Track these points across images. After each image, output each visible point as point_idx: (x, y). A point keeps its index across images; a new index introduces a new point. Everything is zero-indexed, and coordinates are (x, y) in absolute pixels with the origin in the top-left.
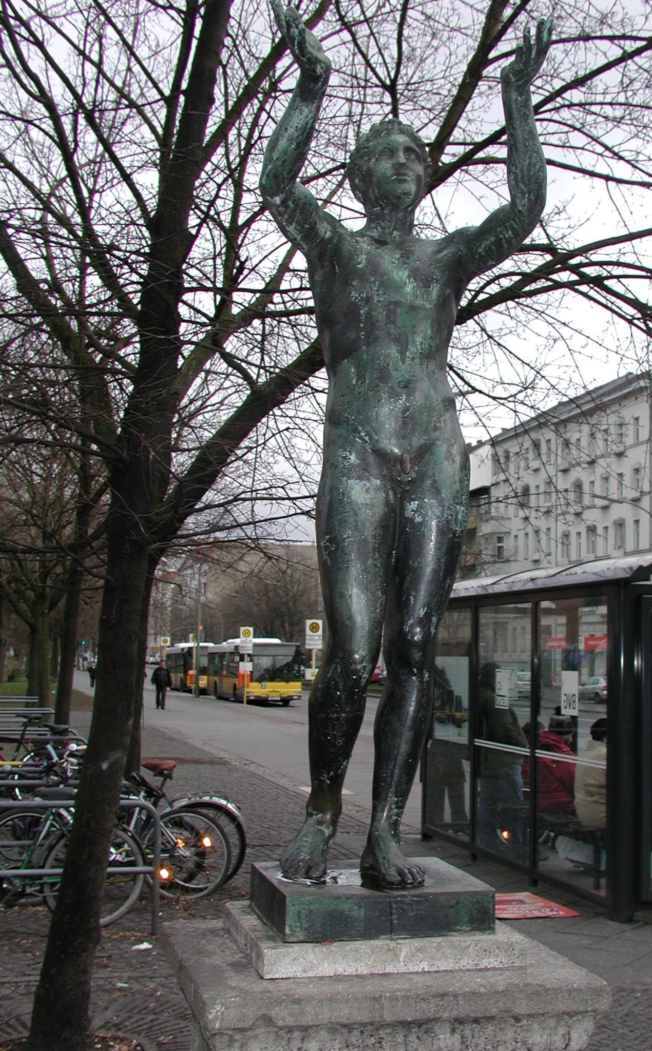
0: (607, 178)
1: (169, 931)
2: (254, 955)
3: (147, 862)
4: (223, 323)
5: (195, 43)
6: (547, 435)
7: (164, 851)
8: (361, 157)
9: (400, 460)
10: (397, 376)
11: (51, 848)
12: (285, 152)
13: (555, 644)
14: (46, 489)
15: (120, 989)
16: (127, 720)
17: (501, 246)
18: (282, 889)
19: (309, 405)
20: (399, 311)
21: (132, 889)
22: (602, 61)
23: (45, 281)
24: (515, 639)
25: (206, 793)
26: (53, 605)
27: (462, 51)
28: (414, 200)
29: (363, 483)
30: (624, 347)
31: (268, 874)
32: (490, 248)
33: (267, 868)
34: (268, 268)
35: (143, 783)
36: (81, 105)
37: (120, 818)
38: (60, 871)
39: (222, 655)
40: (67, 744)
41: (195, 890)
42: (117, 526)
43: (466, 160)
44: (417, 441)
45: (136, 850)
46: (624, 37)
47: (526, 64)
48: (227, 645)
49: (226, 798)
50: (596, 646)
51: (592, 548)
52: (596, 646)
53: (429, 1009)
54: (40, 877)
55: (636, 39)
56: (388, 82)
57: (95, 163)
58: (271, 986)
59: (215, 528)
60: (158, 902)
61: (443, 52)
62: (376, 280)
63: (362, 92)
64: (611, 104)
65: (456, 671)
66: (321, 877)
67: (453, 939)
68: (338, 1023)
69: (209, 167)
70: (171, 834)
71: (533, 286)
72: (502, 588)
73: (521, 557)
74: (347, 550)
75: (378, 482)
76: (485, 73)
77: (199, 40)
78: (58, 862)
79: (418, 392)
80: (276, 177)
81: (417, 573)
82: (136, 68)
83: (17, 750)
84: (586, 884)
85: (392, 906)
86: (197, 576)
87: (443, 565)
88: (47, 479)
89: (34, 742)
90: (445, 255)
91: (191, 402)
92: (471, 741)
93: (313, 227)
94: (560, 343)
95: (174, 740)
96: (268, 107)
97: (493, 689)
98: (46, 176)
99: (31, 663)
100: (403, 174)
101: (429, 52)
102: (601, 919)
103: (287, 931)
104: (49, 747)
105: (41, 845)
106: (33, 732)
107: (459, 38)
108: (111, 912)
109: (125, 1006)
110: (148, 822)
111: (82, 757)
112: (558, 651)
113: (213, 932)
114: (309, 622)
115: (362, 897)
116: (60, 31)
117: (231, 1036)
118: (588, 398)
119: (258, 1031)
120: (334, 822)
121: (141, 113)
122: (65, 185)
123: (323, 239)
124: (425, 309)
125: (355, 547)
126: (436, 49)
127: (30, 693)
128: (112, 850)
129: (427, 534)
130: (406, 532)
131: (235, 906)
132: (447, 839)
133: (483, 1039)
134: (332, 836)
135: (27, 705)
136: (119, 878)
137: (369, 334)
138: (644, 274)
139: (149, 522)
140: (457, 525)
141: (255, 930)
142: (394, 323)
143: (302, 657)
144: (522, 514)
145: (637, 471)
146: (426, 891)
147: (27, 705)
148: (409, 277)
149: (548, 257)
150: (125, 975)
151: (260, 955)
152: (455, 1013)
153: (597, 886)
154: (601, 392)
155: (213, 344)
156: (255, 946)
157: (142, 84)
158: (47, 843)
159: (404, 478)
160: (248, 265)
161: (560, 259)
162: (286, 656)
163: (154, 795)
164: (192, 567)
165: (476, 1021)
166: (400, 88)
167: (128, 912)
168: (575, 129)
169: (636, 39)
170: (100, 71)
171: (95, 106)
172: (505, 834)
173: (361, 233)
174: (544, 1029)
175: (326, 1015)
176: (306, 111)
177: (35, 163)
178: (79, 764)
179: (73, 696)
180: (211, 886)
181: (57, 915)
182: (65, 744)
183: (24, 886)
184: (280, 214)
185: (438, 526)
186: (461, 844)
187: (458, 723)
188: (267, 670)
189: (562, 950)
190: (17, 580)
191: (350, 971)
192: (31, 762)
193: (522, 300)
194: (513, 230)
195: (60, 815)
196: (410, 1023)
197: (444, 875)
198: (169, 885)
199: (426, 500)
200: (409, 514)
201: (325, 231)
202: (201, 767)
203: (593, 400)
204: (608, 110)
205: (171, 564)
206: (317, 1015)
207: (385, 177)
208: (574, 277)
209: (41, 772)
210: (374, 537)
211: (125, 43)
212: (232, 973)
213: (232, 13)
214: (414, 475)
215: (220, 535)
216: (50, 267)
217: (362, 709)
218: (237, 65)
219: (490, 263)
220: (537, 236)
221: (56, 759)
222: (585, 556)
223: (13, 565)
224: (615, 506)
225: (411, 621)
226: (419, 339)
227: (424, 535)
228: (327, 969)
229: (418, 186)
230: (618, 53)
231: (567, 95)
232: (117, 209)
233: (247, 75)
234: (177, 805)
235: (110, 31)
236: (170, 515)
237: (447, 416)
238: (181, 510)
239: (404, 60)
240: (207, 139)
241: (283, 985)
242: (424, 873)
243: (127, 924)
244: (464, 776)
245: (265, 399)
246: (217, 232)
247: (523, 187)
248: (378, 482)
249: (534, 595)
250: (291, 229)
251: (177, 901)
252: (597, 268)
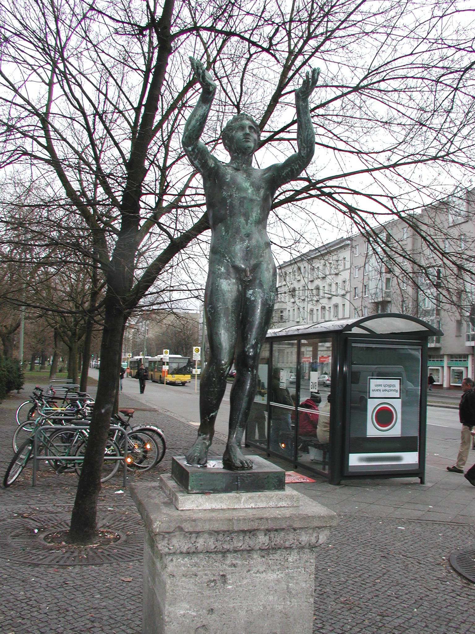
0: (334, 149)
1: (134, 487)
2: (174, 499)
3: (122, 455)
4: (158, 211)
5: (149, 86)
6: (304, 265)
7: (129, 450)
8: (229, 130)
9: (244, 271)
10: (243, 232)
11: (79, 447)
12: (194, 127)
13: (306, 360)
14: (77, 285)
16: (113, 390)
17: (294, 172)
18: (187, 469)
19: (202, 246)
20: (245, 201)
21: (115, 467)
22: (334, 96)
23: (79, 191)
24: (288, 357)
25: (148, 424)
26: (79, 338)
27: (269, 91)
28: (253, 151)
29: (227, 281)
30: (341, 225)
31: (180, 462)
33: (179, 459)
34: (180, 186)
35: (119, 419)
36: (97, 112)
37: (109, 435)
38: (83, 457)
39: (155, 362)
40: (86, 401)
41: (143, 468)
42: (109, 301)
43: (271, 139)
44: (253, 262)
45: (117, 449)
46: (343, 86)
47: (307, 88)
48: (157, 358)
49: (157, 427)
50: (325, 361)
51: (323, 316)
52: (325, 361)
53: (255, 525)
54: (74, 460)
55: (348, 87)
56: (236, 103)
57: (102, 138)
58: (182, 513)
59: (153, 304)
60: (126, 473)
61: (261, 91)
63: (224, 108)
64: (337, 115)
65: (263, 372)
66: (205, 464)
67: (266, 493)
68: (213, 531)
69: (155, 138)
70: (132, 442)
71: (300, 196)
72: (283, 333)
73: (291, 318)
74: (220, 312)
75: (234, 281)
76: (280, 100)
77: (151, 84)
78: (82, 454)
79: (253, 239)
80: (190, 138)
81: (251, 324)
82: (122, 96)
83: (63, 403)
84: (319, 468)
85: (238, 478)
86: (144, 326)
87: (264, 321)
88: (78, 281)
89: (71, 399)
91: (143, 246)
92: (268, 402)
93: (206, 162)
94: (312, 222)
95: (133, 400)
96: (182, 112)
97: (279, 379)
98: (80, 144)
99: (69, 364)
100: (248, 139)
101: (254, 90)
102: (326, 483)
103: (189, 488)
104: (78, 402)
105: (74, 446)
106: (70, 395)
107: (268, 84)
108: (105, 476)
110: (122, 437)
111: (92, 407)
112: (307, 363)
113: (154, 487)
114: (194, 348)
115: (224, 473)
117: (164, 535)
118: (324, 248)
119: (176, 533)
120: (211, 439)
121: (124, 116)
122: (89, 148)
123: (210, 167)
124: (257, 200)
125: (223, 311)
126: (257, 90)
127: (69, 377)
128: (106, 449)
129: (257, 306)
130: (243, 306)
131: (165, 476)
132: (257, 447)
133: (279, 538)
134: (210, 445)
135: (68, 383)
136: (109, 461)
137: (231, 212)
138: (350, 192)
139: (124, 299)
141: (174, 488)
142: (243, 206)
143: (191, 364)
144: (292, 300)
145: (344, 282)
146: (253, 471)
147: (68, 383)
148: (250, 186)
149: (307, 184)
151: (177, 499)
152: (267, 527)
153: (324, 469)
154: (329, 245)
155: (154, 220)
156: (174, 494)
157: (125, 104)
158: (77, 445)
159: (247, 279)
160: (171, 185)
161: (312, 185)
162: (184, 363)
163: (125, 425)
164: (142, 322)
165: (276, 530)
166: (241, 106)
167: (113, 477)
168: (320, 126)
169: (348, 87)
170: (106, 98)
171: (104, 113)
172: (283, 445)
173: (228, 165)
174: (307, 534)
175: (207, 527)
176: (204, 108)
177: (76, 138)
178: (91, 410)
179: (88, 379)
180: (150, 466)
181: (82, 478)
182: (85, 401)
183: (67, 464)
184: (191, 155)
185: (262, 302)
186: (263, 449)
187: (262, 395)
188: (175, 369)
189: (313, 497)
190: (64, 326)
191: (218, 507)
192: (69, 408)
193: (294, 203)
194: (299, 165)
195: (83, 433)
196: (246, 531)
197: (260, 463)
198: (131, 465)
200: (248, 296)
201: (212, 164)
202: (145, 412)
203: (326, 249)
204: (335, 118)
205: (132, 321)
206: (203, 526)
207: (239, 139)
208: (319, 193)
209: (74, 413)
210: (232, 306)
211: (117, 84)
212: (164, 507)
213: (167, 71)
214: (251, 278)
215: (155, 307)
216: (81, 184)
217: (225, 387)
218: (169, 93)
220: (303, 175)
221: (81, 407)
222: (320, 320)
223: (62, 320)
224: (334, 298)
225: (248, 346)
226: (254, 215)
227: (255, 306)
228: (208, 506)
229: (255, 144)
230: (340, 93)
231: (317, 111)
232: (112, 160)
233: (173, 98)
234: (135, 429)
235: (111, 80)
236: (134, 297)
237: (267, 251)
238: (139, 295)
239: (243, 94)
240: (154, 126)
241: (188, 513)
242: (252, 463)
243: (112, 482)
244: (265, 419)
245: (177, 246)
246: (157, 169)
249: (299, 337)
250: (196, 162)
251: (135, 472)
252: (329, 189)
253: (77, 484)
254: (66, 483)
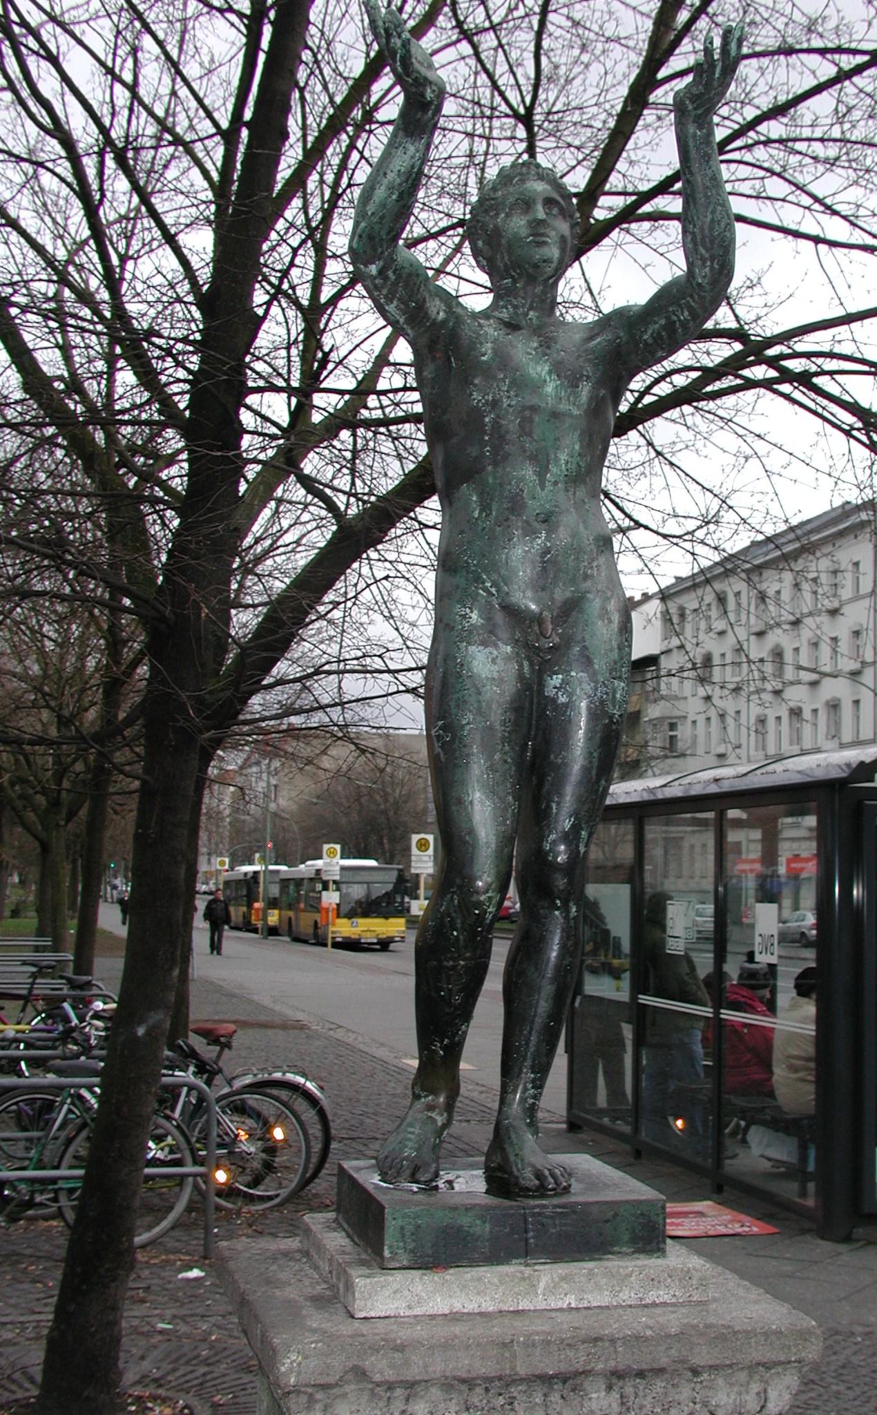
0: (817, 240)
1: (227, 1253)
2: (341, 1286)
3: (197, 1161)
4: (300, 436)
5: (262, 58)
6: (735, 585)
7: (220, 1146)
8: (486, 211)
9: (538, 620)
10: (533, 506)
11: (69, 1141)
12: (383, 205)
13: (746, 867)
14: (62, 658)
16: (171, 969)
17: (674, 331)
18: (380, 1197)
19: (416, 546)
20: (537, 419)
21: (178, 1197)
22: (810, 83)
23: (60, 378)
24: (692, 860)
25: (277, 1068)
26: (71, 815)
27: (621, 68)
28: (556, 270)
29: (488, 650)
30: (840, 467)
31: (360, 1177)
32: (659, 333)
33: (359, 1169)
34: (361, 361)
35: (193, 1054)
36: (109, 141)
37: (161, 1102)
38: (81, 1172)
39: (299, 882)
40: (91, 1002)
41: (262, 1199)
42: (157, 708)
43: (627, 216)
44: (561, 594)
45: (184, 1145)
46: (839, 50)
47: (708, 86)
48: (306, 869)
49: (304, 1075)
50: (802, 869)
51: (797, 737)
52: (802, 869)
53: (578, 1359)
54: (54, 1181)
55: (855, 52)
56: (522, 111)
57: (128, 219)
58: (364, 1328)
59: (290, 711)
60: (213, 1215)
61: (597, 69)
62: (505, 377)
63: (487, 124)
64: (822, 140)
65: (614, 903)
66: (432, 1180)
67: (609, 1264)
68: (454, 1378)
69: (281, 225)
70: (230, 1123)
71: (717, 386)
72: (676, 791)
73: (700, 750)
74: (467, 740)
75: (509, 649)
76: (652, 98)
77: (268, 53)
78: (78, 1161)
79: (562, 528)
80: (371, 238)
81: (560, 772)
82: (183, 92)
83: (23, 1010)
84: (788, 1190)
85: (527, 1220)
86: (265, 776)
87: (595, 761)
88: (63, 644)
89: (46, 998)
90: (599, 343)
91: (258, 541)
92: (634, 997)
93: (421, 306)
94: (754, 462)
95: (234, 996)
96: (360, 144)
97: (663, 928)
98: (61, 237)
99: (41, 893)
100: (543, 235)
101: (577, 70)
102: (808, 1237)
103: (387, 1253)
104: (66, 1005)
105: (56, 1138)
106: (45, 986)
107: (617, 51)
108: (149, 1228)
110: (200, 1107)
111: (110, 1019)
112: (751, 876)
113: (286, 1254)
114: (415, 838)
115: (487, 1208)
117: (311, 1395)
118: (791, 536)
119: (347, 1388)
120: (449, 1107)
121: (190, 152)
122: (87, 249)
123: (434, 322)
124: (571, 416)
125: (478, 737)
126: (587, 66)
127: (40, 933)
128: (151, 1144)
129: (575, 719)
130: (547, 716)
131: (316, 1220)
132: (602, 1129)
133: (649, 1398)
134: (447, 1125)
135: (37, 949)
136: (160, 1183)
137: (496, 450)
138: (866, 368)
139: (200, 703)
140: (614, 706)
141: (344, 1253)
142: (530, 435)
143: (406, 885)
144: (702, 692)
145: (857, 633)
146: (573, 1199)
147: (37, 949)
148: (550, 372)
149: (738, 347)
151: (349, 1286)
152: (613, 1363)
153: (803, 1193)
154: (808, 527)
155: (287, 463)
156: (343, 1273)
157: (191, 114)
158: (63, 1134)
159: (543, 644)
160: (334, 357)
161: (754, 349)
162: (384, 883)
163: (206, 1070)
164: (258, 763)
165: (641, 1374)
166: (538, 118)
167: (172, 1228)
168: (773, 173)
169: (855, 52)
170: (135, 96)
171: (127, 142)
172: (680, 1123)
173: (485, 314)
174: (731, 1385)
175: (439, 1366)
176: (412, 149)
177: (47, 219)
178: (106, 1029)
179: (98, 937)
180: (284, 1193)
181: (77, 1232)
182: (88, 1002)
183: (33, 1193)
184: (376, 287)
185: (589, 709)
186: (620, 1136)
187: (616, 974)
188: (359, 902)
189: (756, 1279)
190: (23, 781)
191: (471, 1307)
192: (42, 1026)
193: (702, 404)
194: (690, 309)
195: (81, 1098)
196: (552, 1377)
197: (597, 1177)
198: (228, 1192)
199: (573, 674)
200: (550, 692)
201: (437, 311)
202: (270, 1032)
203: (798, 539)
204: (818, 148)
205: (230, 760)
206: (426, 1366)
207: (517, 239)
208: (772, 373)
209: (56, 1040)
210: (504, 723)
211: (168, 57)
212: (312, 1311)
213: (312, 17)
214: (557, 640)
215: (295, 720)
216: (68, 359)
217: (487, 954)
218: (319, 88)
219: (659, 354)
220: (723, 318)
221: (75, 1021)
222: (786, 748)
223: (17, 760)
224: (827, 682)
225: (553, 837)
226: (563, 457)
227: (570, 721)
228: (440, 1305)
229: (563, 250)
230: (832, 71)
231: (762, 128)
232: (157, 281)
233: (332, 101)
234: (238, 1084)
235: (147, 42)
236: (228, 693)
237: (602, 560)
238: (244, 687)
239: (544, 81)
240: (279, 186)
241: (381, 1327)
242: (570, 1175)
243: (171, 1244)
244: (624, 1045)
245: (357, 537)
246: (292, 313)
247: (703, 251)
248: (509, 649)
249: (718, 801)
250: (391, 308)
251: (239, 1213)
252: (803, 360)
253: (62, 1253)
254: (28, 1251)
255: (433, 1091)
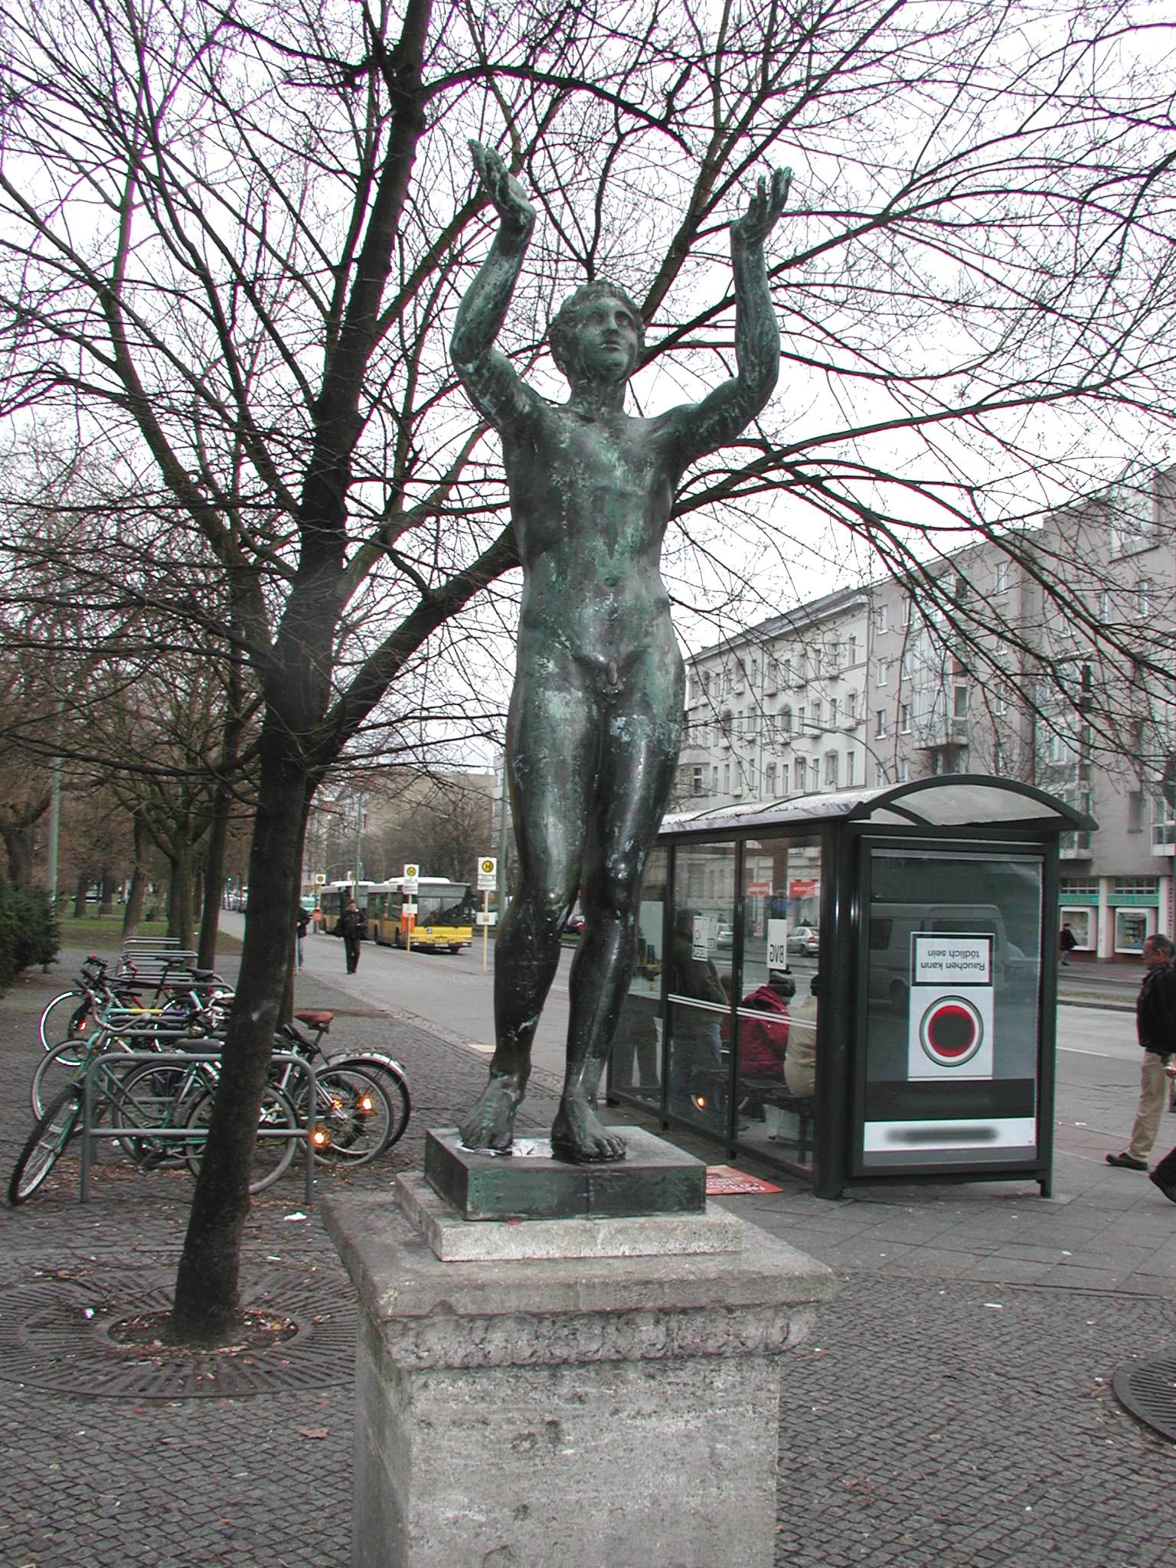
0: (828, 368)
1: (332, 1204)
2: (430, 1234)
3: (301, 1125)
4: (392, 521)
5: (368, 212)
6: (752, 655)
7: (319, 1113)
8: (566, 323)
9: (605, 669)
10: (602, 573)
11: (195, 1106)
12: (480, 313)
13: (757, 889)
14: (191, 704)
15: (271, 1263)
16: (281, 965)
17: (727, 426)
18: (464, 1160)
19: (499, 608)
20: (607, 497)
21: (284, 1154)
22: (826, 237)
23: (195, 472)
24: (712, 883)
25: (367, 1050)
26: (197, 836)
27: (666, 224)
28: (626, 372)
29: (563, 694)
30: (843, 555)
31: (446, 1143)
33: (444, 1136)
34: (445, 460)
35: (296, 1037)
36: (240, 276)
37: (271, 1075)
38: (205, 1131)
39: (383, 896)
40: (212, 992)
41: (353, 1157)
42: (271, 745)
43: (670, 343)
44: (626, 648)
45: (289, 1112)
46: (848, 214)
47: (760, 218)
48: (390, 885)
49: (388, 1055)
50: (804, 892)
51: (801, 782)
52: (804, 892)
53: (631, 1299)
54: (183, 1137)
55: (861, 216)
56: (584, 256)
57: (254, 342)
58: (451, 1270)
59: (378, 752)
60: (313, 1169)
61: (646, 224)
63: (554, 267)
64: (834, 285)
65: (651, 919)
66: (507, 1147)
67: (658, 1219)
68: (526, 1312)
69: (383, 342)
70: (328, 1094)
71: (743, 486)
72: (702, 825)
73: (721, 788)
74: (543, 773)
75: (580, 694)
76: (692, 248)
77: (374, 209)
78: (202, 1123)
79: (627, 592)
80: (469, 341)
81: (622, 800)
82: (303, 238)
83: (157, 997)
84: (790, 1157)
85: (590, 1183)
86: (356, 807)
87: (653, 793)
88: (192, 694)
89: (175, 987)
91: (354, 609)
92: (664, 995)
93: (510, 400)
94: (772, 550)
95: (330, 989)
96: (451, 277)
97: (690, 938)
98: (198, 357)
99: (171, 901)
100: (615, 343)
101: (630, 223)
102: (806, 1196)
103: (469, 1208)
104: (192, 993)
105: (184, 1103)
106: (174, 977)
107: (663, 209)
108: (260, 1178)
109: (277, 1282)
110: (301, 1081)
111: (228, 1006)
112: (761, 898)
113: (381, 1206)
114: (481, 860)
115: (554, 1171)
116: (219, 198)
117: (405, 1324)
118: (802, 613)
119: (436, 1319)
120: (522, 1086)
121: (306, 286)
122: (219, 366)
123: (521, 413)
124: (637, 496)
125: (552, 770)
126: (637, 222)
127: (171, 933)
128: (263, 1110)
129: (635, 756)
130: (603, 756)
131: (408, 1178)
132: (636, 1105)
133: (691, 1331)
134: (519, 1101)
135: (168, 947)
136: (270, 1141)
137: (571, 524)
138: (866, 474)
139: (307, 740)
141: (431, 1206)
142: (601, 510)
143: (473, 899)
144: (724, 742)
145: (852, 697)
146: (627, 1165)
147: (168, 947)
148: (619, 459)
149: (759, 454)
150: (277, 1248)
151: (437, 1234)
152: (660, 1303)
153: (802, 1160)
154: (816, 606)
155: (382, 544)
156: (431, 1223)
157: (309, 256)
158: (190, 1100)
159: (610, 691)
160: (423, 456)
161: (773, 457)
162: (454, 898)
163: (309, 1050)
164: (350, 797)
165: (684, 1311)
166: (597, 262)
167: (279, 1179)
168: (793, 311)
169: (861, 216)
170: (263, 242)
171: (256, 279)
172: (701, 1101)
173: (564, 408)
174: (760, 1320)
175: (513, 1303)
176: (506, 266)
177: (187, 342)
178: (225, 1014)
179: (218, 938)
180: (371, 1152)
181: (203, 1183)
182: (209, 992)
183: (165, 1147)
184: (473, 383)
185: (648, 746)
186: (651, 1111)
187: (649, 976)
188: (433, 913)
189: (775, 1230)
190: (158, 807)
191: (541, 1253)
192: (172, 1010)
193: (729, 501)
194: (741, 407)
195: (204, 1070)
196: (609, 1313)
197: (645, 1146)
198: (325, 1151)
200: (614, 731)
201: (524, 405)
202: (359, 1020)
203: (808, 615)
204: (829, 293)
205: (328, 794)
206: (503, 1302)
207: (592, 345)
208: (789, 477)
209: (184, 1022)
210: (575, 758)
211: (291, 208)
212: (405, 1254)
213: (413, 174)
214: (621, 687)
215: (383, 760)
216: (201, 456)
217: (556, 956)
218: (417, 231)
220: (751, 432)
221: (200, 1007)
222: (792, 791)
223: (153, 790)
224: (827, 736)
225: (615, 856)
226: (629, 531)
227: (631, 757)
228: (514, 1251)
229: (631, 356)
230: (843, 231)
231: (784, 274)
232: (278, 394)
233: (428, 242)
234: (334, 1062)
235: (274, 197)
236: (331, 734)
237: (661, 620)
238: (344, 729)
239: (602, 232)
240: (382, 311)
241: (464, 1269)
242: (625, 1144)
243: (278, 1192)
244: (656, 1035)
245: (438, 607)
246: (388, 418)
249: (739, 833)
250: (485, 401)
251: (334, 1168)
252: (814, 467)
255: (510, 1073)
